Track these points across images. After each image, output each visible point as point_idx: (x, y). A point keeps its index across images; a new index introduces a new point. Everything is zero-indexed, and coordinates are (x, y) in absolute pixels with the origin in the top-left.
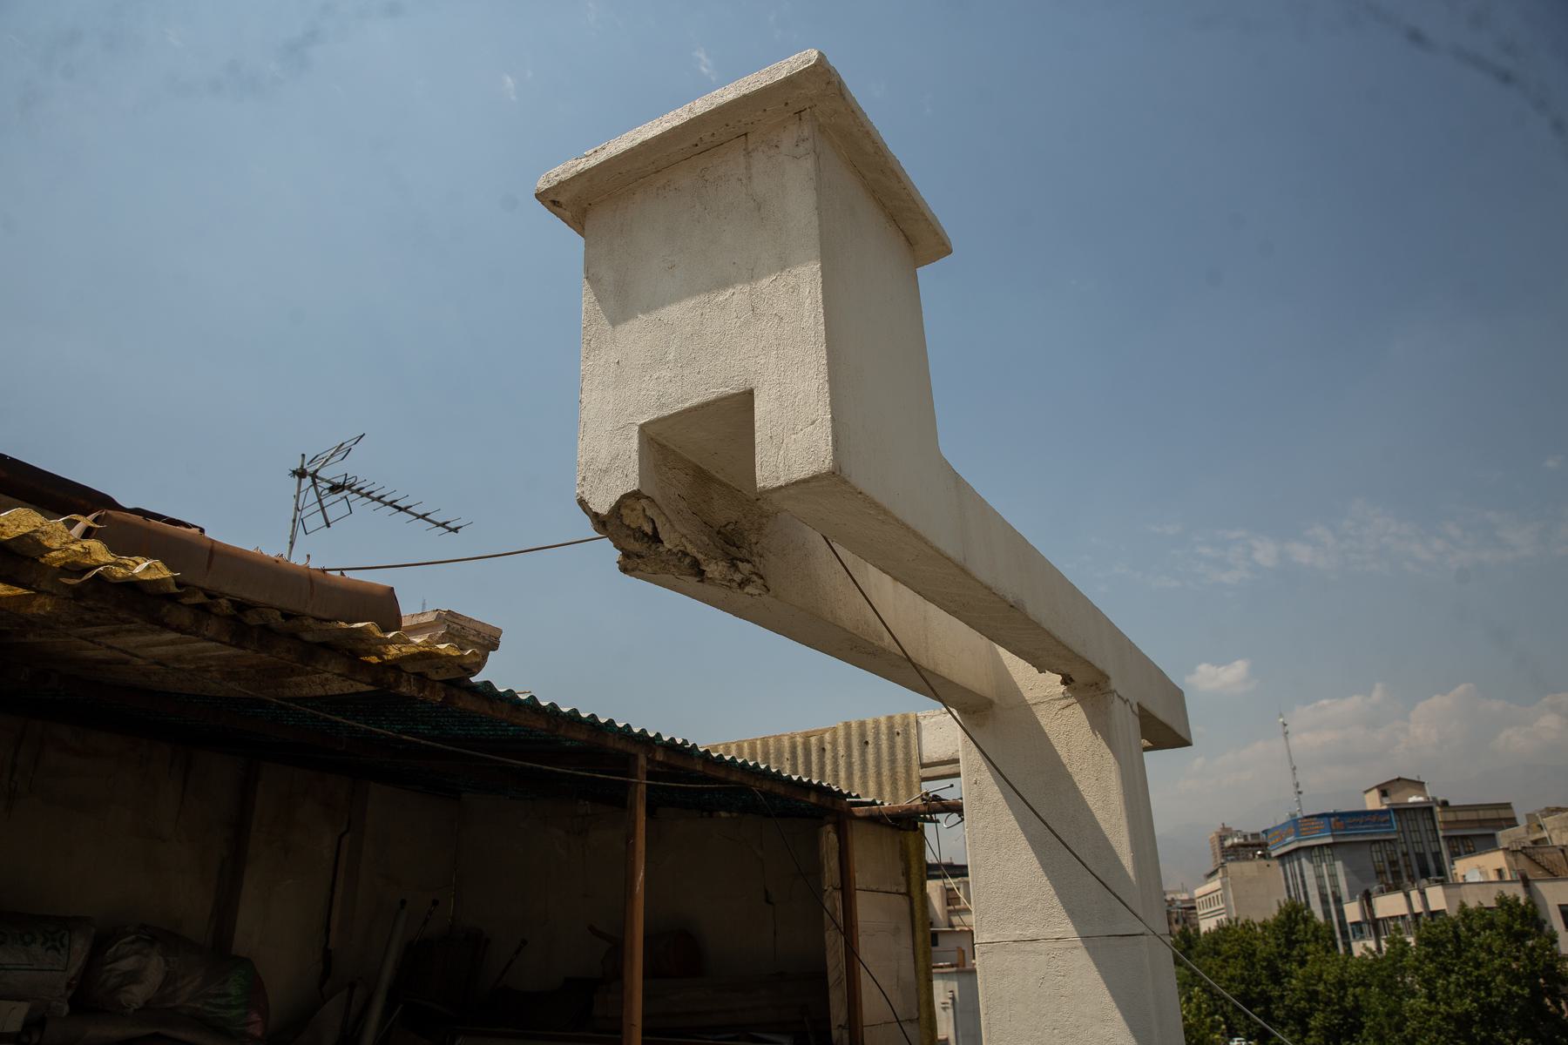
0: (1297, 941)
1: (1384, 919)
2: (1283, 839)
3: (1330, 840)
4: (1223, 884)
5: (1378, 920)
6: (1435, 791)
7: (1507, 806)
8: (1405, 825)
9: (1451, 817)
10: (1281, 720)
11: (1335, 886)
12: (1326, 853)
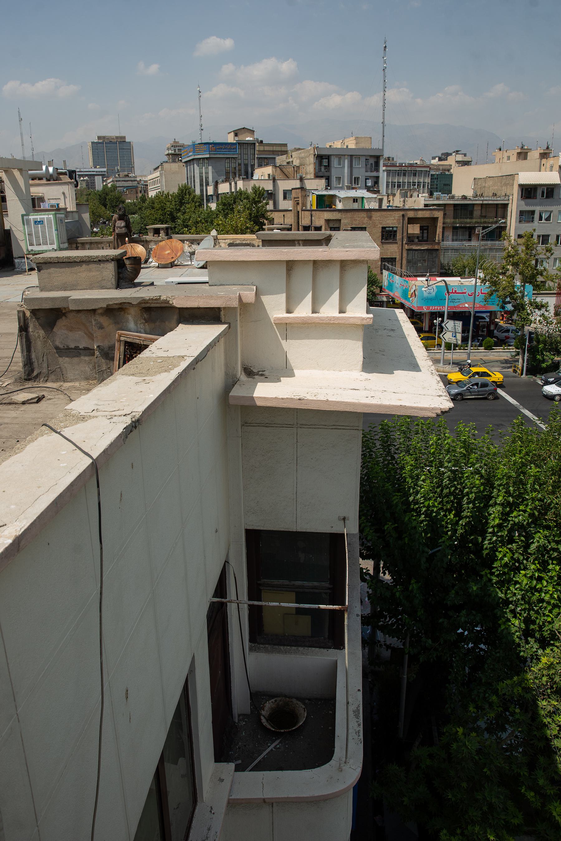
0: (184, 203)
1: (221, 194)
2: (188, 154)
3: (208, 156)
4: (160, 174)
5: (219, 194)
6: (258, 136)
7: (285, 145)
8: (242, 151)
9: (262, 148)
10: (198, 89)
11: (207, 178)
12: (205, 162)
